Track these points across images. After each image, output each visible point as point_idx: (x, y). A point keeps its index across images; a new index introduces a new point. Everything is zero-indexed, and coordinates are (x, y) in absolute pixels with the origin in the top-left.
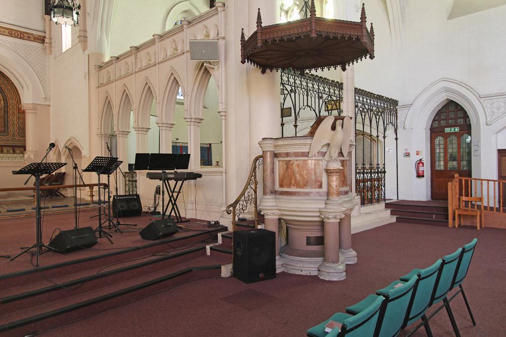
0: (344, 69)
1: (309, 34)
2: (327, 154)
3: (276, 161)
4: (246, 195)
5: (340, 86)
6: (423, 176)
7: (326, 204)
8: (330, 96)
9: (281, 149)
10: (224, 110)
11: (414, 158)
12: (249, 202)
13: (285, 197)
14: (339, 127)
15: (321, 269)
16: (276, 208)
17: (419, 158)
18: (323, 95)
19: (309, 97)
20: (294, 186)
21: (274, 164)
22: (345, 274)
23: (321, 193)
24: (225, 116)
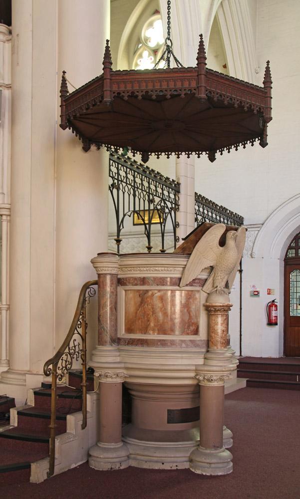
0: (212, 159)
1: (194, 94)
2: (210, 281)
3: (121, 291)
4: (71, 344)
5: (176, 187)
6: (276, 324)
7: (205, 358)
8: (164, 200)
9: (133, 272)
10: (8, 206)
11: (265, 299)
12: (75, 356)
13: (139, 348)
14: (230, 242)
15: (194, 458)
16: (122, 365)
17: (270, 298)
18: (155, 197)
19: (137, 199)
20: (154, 330)
21: (117, 295)
22: (231, 464)
23: (198, 342)
24: (10, 215)
